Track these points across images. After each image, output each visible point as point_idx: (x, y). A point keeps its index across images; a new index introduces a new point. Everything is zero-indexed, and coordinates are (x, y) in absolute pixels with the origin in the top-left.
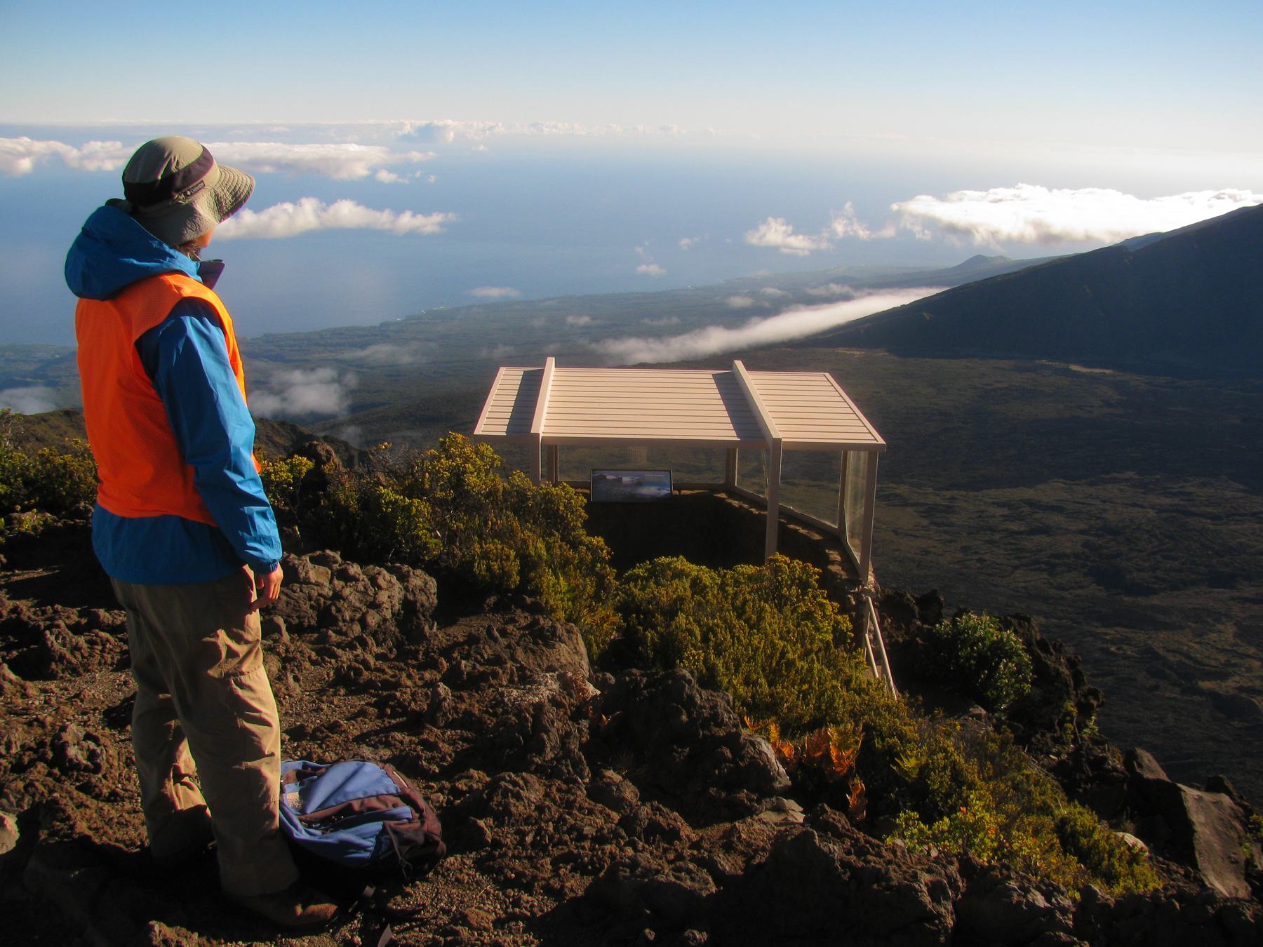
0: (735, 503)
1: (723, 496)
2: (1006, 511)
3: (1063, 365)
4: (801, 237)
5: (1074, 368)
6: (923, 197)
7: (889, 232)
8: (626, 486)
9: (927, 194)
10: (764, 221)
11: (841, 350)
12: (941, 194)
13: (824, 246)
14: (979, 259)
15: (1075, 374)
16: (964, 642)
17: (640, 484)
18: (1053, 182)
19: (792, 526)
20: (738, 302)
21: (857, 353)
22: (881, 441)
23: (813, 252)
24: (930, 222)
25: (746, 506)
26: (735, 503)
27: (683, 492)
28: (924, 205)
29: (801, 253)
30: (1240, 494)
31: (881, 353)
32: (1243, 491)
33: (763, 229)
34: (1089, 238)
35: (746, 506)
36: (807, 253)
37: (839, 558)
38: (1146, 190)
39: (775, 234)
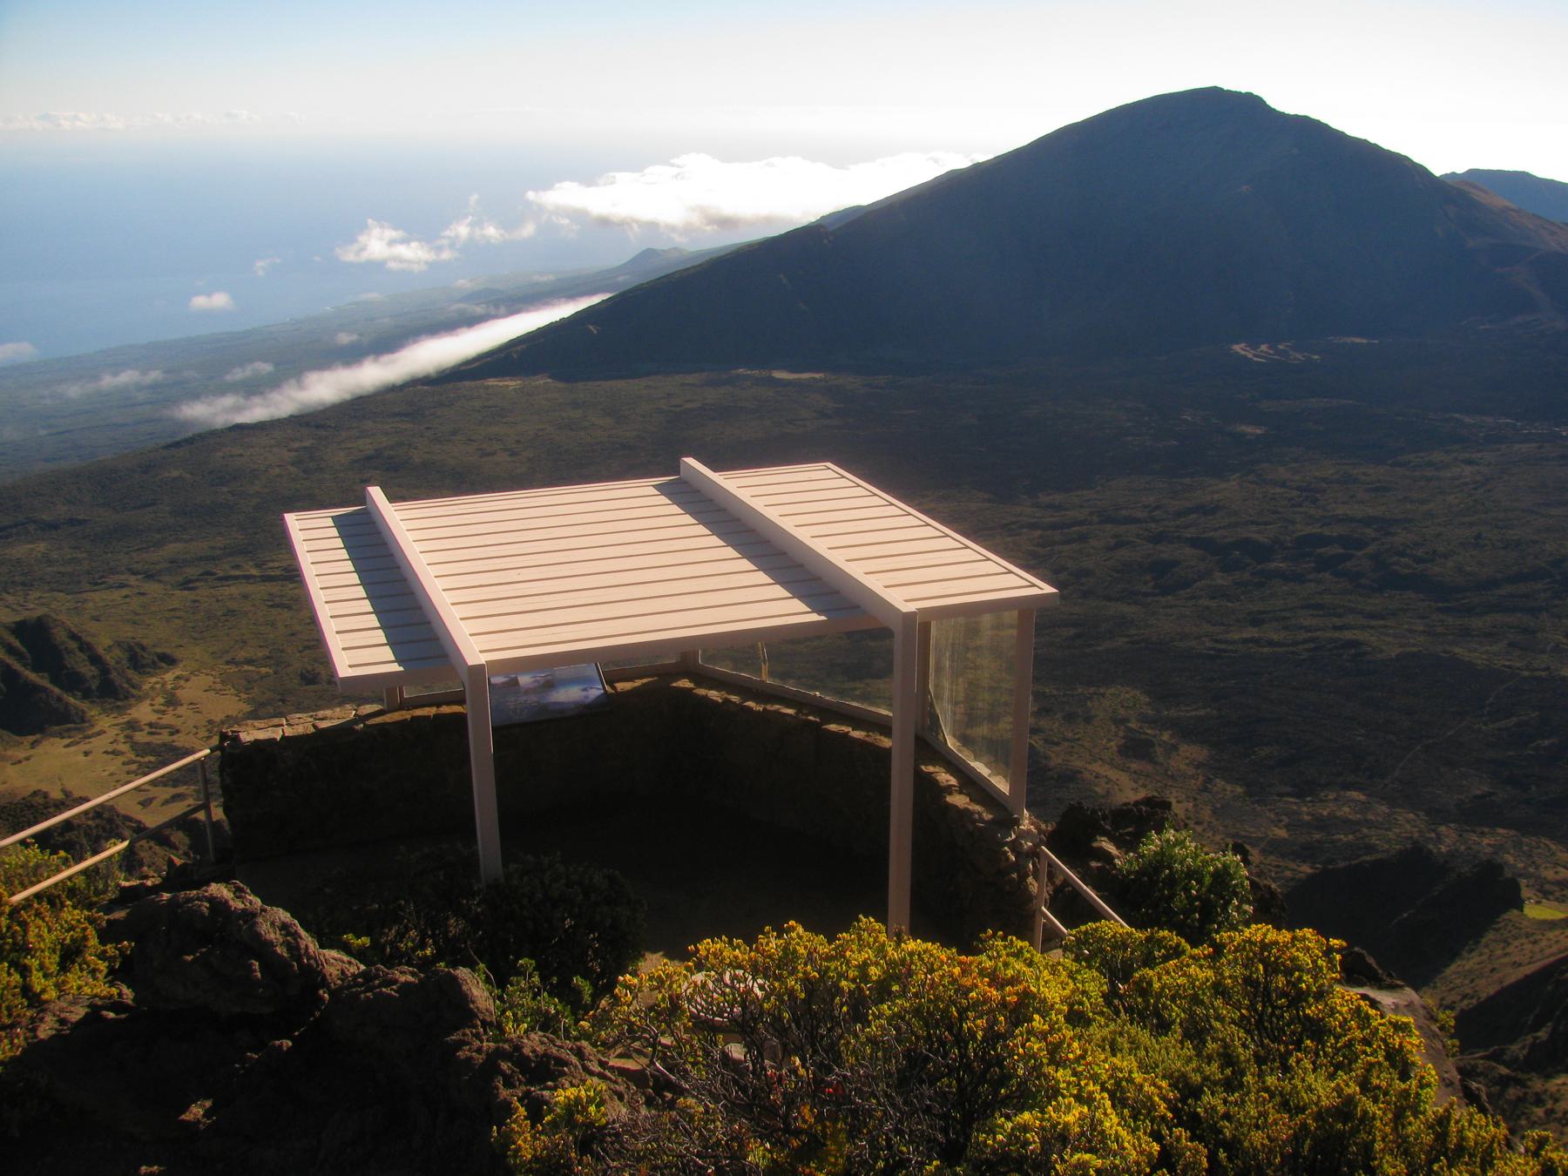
0: (714, 694)
1: (685, 683)
2: (1072, 631)
3: (764, 373)
4: (414, 244)
5: (779, 375)
6: (567, 184)
7: (528, 230)
8: (528, 691)
9: (571, 180)
10: (364, 228)
11: (492, 382)
12: (589, 178)
13: (446, 255)
14: (649, 254)
15: (781, 383)
16: (1171, 882)
17: (550, 685)
18: (731, 151)
19: (833, 727)
20: (344, 339)
21: (512, 384)
22: (1049, 589)
23: (432, 265)
24: (579, 216)
25: (734, 698)
26: (714, 694)
27: (621, 686)
28: (567, 196)
29: (416, 268)
30: (987, 505)
31: (541, 381)
32: (989, 501)
33: (363, 239)
34: (769, 220)
35: (734, 698)
36: (424, 267)
37: (953, 781)
38: (840, 157)
39: (377, 244)
